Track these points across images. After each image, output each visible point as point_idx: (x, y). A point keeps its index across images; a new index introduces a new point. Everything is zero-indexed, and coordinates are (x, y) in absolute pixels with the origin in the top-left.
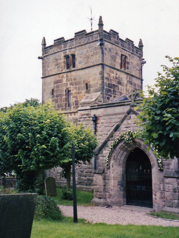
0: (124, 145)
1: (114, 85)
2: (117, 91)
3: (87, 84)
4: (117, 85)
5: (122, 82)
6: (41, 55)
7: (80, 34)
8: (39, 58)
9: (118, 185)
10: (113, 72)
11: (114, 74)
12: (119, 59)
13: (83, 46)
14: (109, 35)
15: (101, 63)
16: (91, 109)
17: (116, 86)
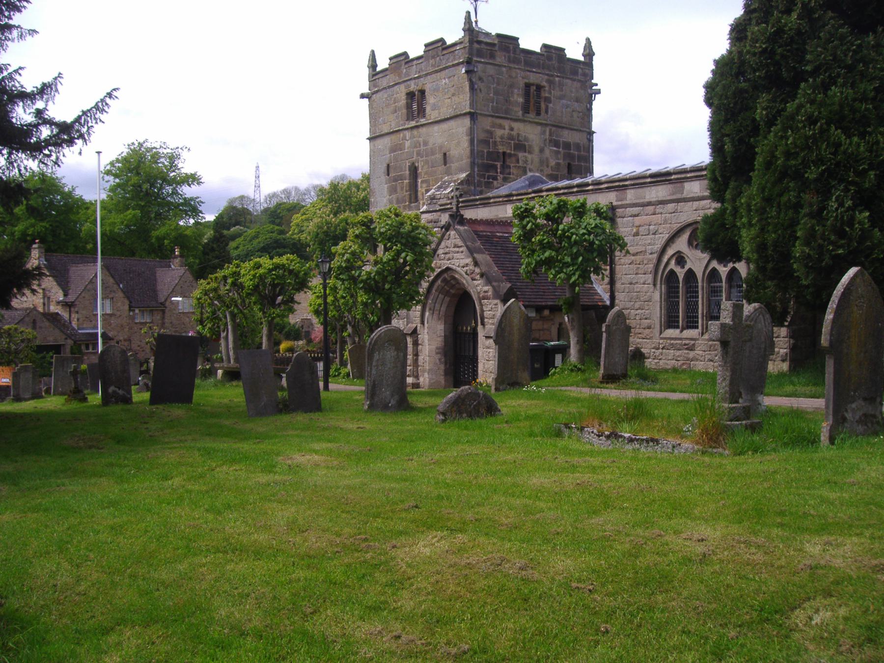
0: (443, 285)
1: (504, 153)
2: (512, 165)
3: (445, 154)
4: (513, 152)
5: (526, 144)
6: (366, 90)
7: (437, 47)
8: (363, 96)
9: (437, 353)
10: (501, 127)
11: (505, 129)
12: (518, 95)
13: (439, 74)
14: (489, 48)
15: (468, 110)
16: (440, 210)
17: (510, 155)
